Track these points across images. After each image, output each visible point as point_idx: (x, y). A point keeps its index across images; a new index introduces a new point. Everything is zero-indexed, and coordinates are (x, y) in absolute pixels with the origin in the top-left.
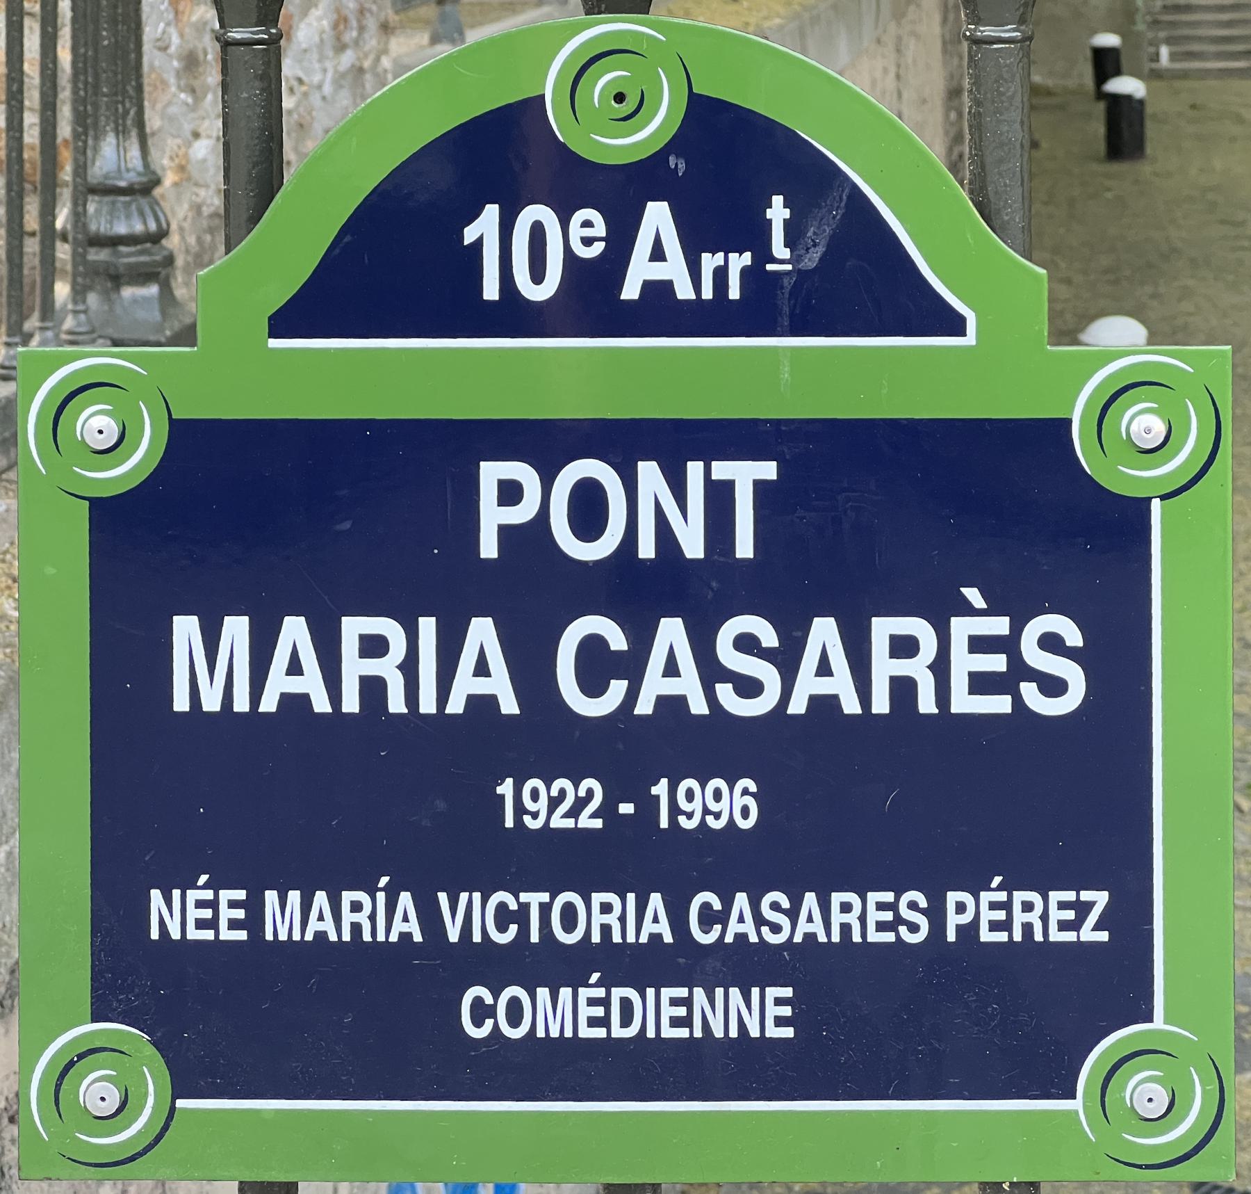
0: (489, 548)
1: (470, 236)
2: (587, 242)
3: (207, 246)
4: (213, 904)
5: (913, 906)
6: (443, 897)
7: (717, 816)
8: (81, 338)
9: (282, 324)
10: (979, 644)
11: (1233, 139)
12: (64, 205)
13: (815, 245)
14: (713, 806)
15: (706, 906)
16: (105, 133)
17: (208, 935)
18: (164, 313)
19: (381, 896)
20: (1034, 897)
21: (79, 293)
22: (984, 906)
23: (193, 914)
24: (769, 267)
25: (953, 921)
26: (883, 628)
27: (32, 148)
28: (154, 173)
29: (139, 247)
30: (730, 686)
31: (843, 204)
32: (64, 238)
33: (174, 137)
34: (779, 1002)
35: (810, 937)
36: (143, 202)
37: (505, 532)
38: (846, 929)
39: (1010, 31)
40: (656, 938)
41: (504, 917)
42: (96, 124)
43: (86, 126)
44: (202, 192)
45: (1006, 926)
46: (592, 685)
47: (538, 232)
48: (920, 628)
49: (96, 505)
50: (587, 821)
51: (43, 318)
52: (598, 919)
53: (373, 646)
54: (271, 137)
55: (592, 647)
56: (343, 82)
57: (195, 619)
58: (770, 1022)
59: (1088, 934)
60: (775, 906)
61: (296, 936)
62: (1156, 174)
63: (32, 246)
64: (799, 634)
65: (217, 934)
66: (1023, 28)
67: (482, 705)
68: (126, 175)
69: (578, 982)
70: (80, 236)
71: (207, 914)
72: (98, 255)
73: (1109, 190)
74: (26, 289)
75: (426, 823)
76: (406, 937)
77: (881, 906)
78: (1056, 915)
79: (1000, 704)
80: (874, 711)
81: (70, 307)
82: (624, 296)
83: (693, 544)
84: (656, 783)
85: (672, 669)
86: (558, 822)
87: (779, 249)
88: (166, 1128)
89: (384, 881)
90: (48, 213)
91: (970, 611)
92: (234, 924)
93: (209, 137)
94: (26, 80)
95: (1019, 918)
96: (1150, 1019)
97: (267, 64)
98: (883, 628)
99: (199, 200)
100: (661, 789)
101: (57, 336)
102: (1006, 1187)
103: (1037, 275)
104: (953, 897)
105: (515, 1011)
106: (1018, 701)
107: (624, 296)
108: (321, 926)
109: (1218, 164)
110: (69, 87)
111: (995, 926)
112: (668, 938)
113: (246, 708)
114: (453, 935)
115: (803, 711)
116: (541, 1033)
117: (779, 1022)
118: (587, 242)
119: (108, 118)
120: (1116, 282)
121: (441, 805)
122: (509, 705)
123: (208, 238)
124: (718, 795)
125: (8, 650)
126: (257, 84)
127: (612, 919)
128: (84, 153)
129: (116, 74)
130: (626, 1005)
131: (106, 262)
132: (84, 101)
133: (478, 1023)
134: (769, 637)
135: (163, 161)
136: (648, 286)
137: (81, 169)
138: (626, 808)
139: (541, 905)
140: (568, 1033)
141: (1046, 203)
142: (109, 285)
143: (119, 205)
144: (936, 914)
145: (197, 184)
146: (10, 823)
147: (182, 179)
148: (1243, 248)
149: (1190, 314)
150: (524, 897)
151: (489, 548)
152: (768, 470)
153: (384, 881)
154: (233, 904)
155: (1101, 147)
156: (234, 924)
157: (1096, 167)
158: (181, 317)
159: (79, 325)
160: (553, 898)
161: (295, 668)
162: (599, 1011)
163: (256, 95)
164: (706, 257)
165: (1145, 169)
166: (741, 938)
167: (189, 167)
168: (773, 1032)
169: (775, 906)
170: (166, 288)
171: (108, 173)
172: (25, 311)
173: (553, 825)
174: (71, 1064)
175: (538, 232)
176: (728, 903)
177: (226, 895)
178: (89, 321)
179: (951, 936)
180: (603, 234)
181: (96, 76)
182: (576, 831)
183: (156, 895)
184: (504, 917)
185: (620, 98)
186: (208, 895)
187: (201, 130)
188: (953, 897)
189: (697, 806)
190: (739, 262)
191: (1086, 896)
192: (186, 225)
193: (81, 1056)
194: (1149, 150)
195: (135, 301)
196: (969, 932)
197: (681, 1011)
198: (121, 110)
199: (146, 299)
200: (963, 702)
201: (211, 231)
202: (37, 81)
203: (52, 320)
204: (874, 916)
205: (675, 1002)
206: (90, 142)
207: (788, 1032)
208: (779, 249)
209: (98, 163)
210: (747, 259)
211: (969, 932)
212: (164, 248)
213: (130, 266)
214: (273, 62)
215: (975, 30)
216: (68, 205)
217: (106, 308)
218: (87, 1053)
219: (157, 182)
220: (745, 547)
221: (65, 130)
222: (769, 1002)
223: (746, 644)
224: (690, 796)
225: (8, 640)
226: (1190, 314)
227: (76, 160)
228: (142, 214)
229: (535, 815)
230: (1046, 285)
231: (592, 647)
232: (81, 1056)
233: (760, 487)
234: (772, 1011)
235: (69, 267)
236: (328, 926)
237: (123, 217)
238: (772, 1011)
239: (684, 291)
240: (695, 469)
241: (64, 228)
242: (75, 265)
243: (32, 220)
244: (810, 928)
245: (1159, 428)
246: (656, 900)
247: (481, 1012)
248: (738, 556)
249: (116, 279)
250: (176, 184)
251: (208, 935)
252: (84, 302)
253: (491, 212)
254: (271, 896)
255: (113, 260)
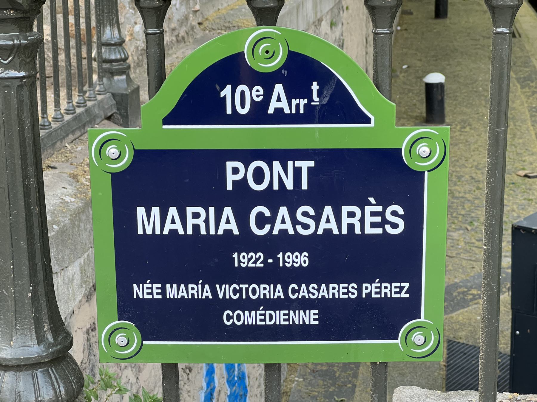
0: (229, 187)
1: (222, 94)
2: (258, 96)
3: (140, 60)
4: (152, 288)
5: (353, 288)
6: (217, 286)
7: (297, 263)
8: (102, 93)
9: (167, 121)
10: (373, 214)
11: (477, 11)
12: (94, 49)
13: (326, 97)
14: (295, 260)
15: (293, 288)
16: (107, 26)
17: (151, 297)
18: (128, 84)
19: (200, 286)
20: (388, 285)
21: (100, 78)
22: (373, 287)
23: (146, 291)
24: (312, 103)
25: (364, 292)
26: (345, 209)
27: (83, 30)
28: (123, 38)
29: (119, 63)
30: (300, 226)
31: (335, 84)
32: (95, 60)
33: (129, 24)
34: (314, 314)
35: (323, 297)
36: (120, 48)
37: (234, 182)
38: (334, 294)
39: (386, 31)
40: (279, 297)
41: (235, 291)
42: (103, 23)
43: (100, 24)
44: (138, 42)
45: (380, 293)
46: (260, 226)
47: (243, 93)
48: (356, 210)
49: (113, 174)
50: (259, 265)
51: (90, 87)
52: (262, 292)
53: (196, 215)
54: (162, 63)
55: (260, 215)
56: (183, 3)
57: (144, 207)
58: (312, 320)
59: (403, 295)
60: (313, 288)
61: (176, 297)
62: (450, 23)
63: (85, 62)
64: (321, 211)
65: (153, 296)
66: (390, 29)
67: (228, 232)
68: (114, 40)
69: (258, 309)
70: (100, 60)
71: (150, 291)
72: (106, 66)
73: (435, 29)
74: (84, 76)
75: (212, 265)
76: (207, 297)
77: (344, 288)
78: (394, 290)
79: (379, 231)
80: (342, 233)
81: (98, 83)
82: (269, 112)
83: (289, 185)
84: (279, 254)
85: (283, 221)
86: (250, 265)
87: (315, 98)
88: (140, 349)
89: (200, 282)
90: (89, 52)
91: (371, 204)
92: (158, 294)
93: (140, 24)
94: (80, 8)
95: (383, 291)
96: (420, 318)
97: (160, 40)
98: (345, 209)
99: (138, 45)
100: (280, 255)
101: (94, 92)
102: (378, 363)
103: (392, 106)
104: (364, 285)
105: (239, 318)
106: (384, 230)
107: (269, 112)
108: (183, 294)
109: (471, 20)
110: (94, 9)
111: (376, 293)
112: (283, 297)
113: (159, 233)
114: (221, 297)
115: (322, 233)
116: (246, 323)
117: (315, 320)
118: (258, 96)
119: (107, 21)
120: (436, 60)
121: (217, 260)
122: (236, 232)
123: (141, 57)
124: (297, 257)
125: (84, 194)
126: (156, 46)
127: (266, 292)
128: (100, 32)
129: (109, 6)
130: (271, 316)
131: (109, 68)
132: (99, 15)
133: (228, 320)
134: (312, 212)
135: (125, 32)
136: (276, 109)
137: (99, 38)
138: (270, 261)
139: (246, 288)
140: (254, 323)
141: (414, 34)
142: (110, 75)
143: (112, 49)
144: (360, 290)
145: (136, 40)
146: (88, 246)
147: (131, 38)
148: (479, 48)
149: (460, 71)
150: (241, 286)
151: (229, 187)
152: (312, 164)
153: (200, 282)
154: (157, 288)
155: (433, 14)
156: (158, 294)
157: (431, 21)
158: (133, 86)
159: (101, 88)
160: (249, 286)
161: (173, 222)
162: (263, 317)
163: (156, 50)
164: (293, 100)
165: (447, 21)
166: (303, 297)
167: (134, 34)
168: (312, 322)
169: (313, 288)
170: (128, 76)
171: (108, 39)
172: (84, 84)
173: (249, 266)
174: (113, 332)
175: (243, 93)
176: (300, 287)
177: (155, 286)
178: (104, 87)
179: (364, 296)
180: (262, 94)
181: (103, 7)
182: (256, 267)
183: (135, 286)
184: (235, 291)
185: (267, 52)
186: (150, 286)
187: (137, 22)
188: (364, 285)
189: (291, 260)
190: (303, 102)
191: (403, 284)
192: (134, 53)
193: (115, 330)
194: (449, 15)
195: (118, 80)
196: (369, 295)
197: (286, 317)
198: (111, 18)
199: (122, 80)
200: (368, 230)
201: (142, 55)
202: (84, 8)
203: (93, 87)
204: (342, 290)
205: (284, 315)
206: (102, 29)
207: (317, 323)
208: (315, 98)
209: (104, 36)
210: (306, 101)
211: (369, 295)
212: (127, 63)
213: (117, 69)
214: (161, 39)
215: (376, 30)
216: (96, 49)
217: (109, 83)
218: (117, 329)
219: (124, 41)
220: (305, 186)
221: (93, 24)
222: (311, 314)
223: (305, 214)
224: (289, 257)
225: (84, 191)
226: (460, 71)
227: (97, 35)
228: (119, 52)
229: (244, 263)
230: (395, 109)
231: (260, 215)
232: (115, 330)
233: (309, 169)
234: (312, 317)
235: (97, 70)
236: (185, 294)
237: (113, 53)
238: (312, 317)
239: (287, 111)
240: (290, 164)
241: (95, 57)
242: (99, 70)
243: (84, 54)
244: (323, 294)
245: (428, 151)
246: (279, 287)
247: (229, 318)
248: (303, 189)
249: (112, 73)
250: (130, 40)
251: (151, 297)
252: (102, 81)
253: (229, 87)
254: (168, 286)
255: (111, 67)
